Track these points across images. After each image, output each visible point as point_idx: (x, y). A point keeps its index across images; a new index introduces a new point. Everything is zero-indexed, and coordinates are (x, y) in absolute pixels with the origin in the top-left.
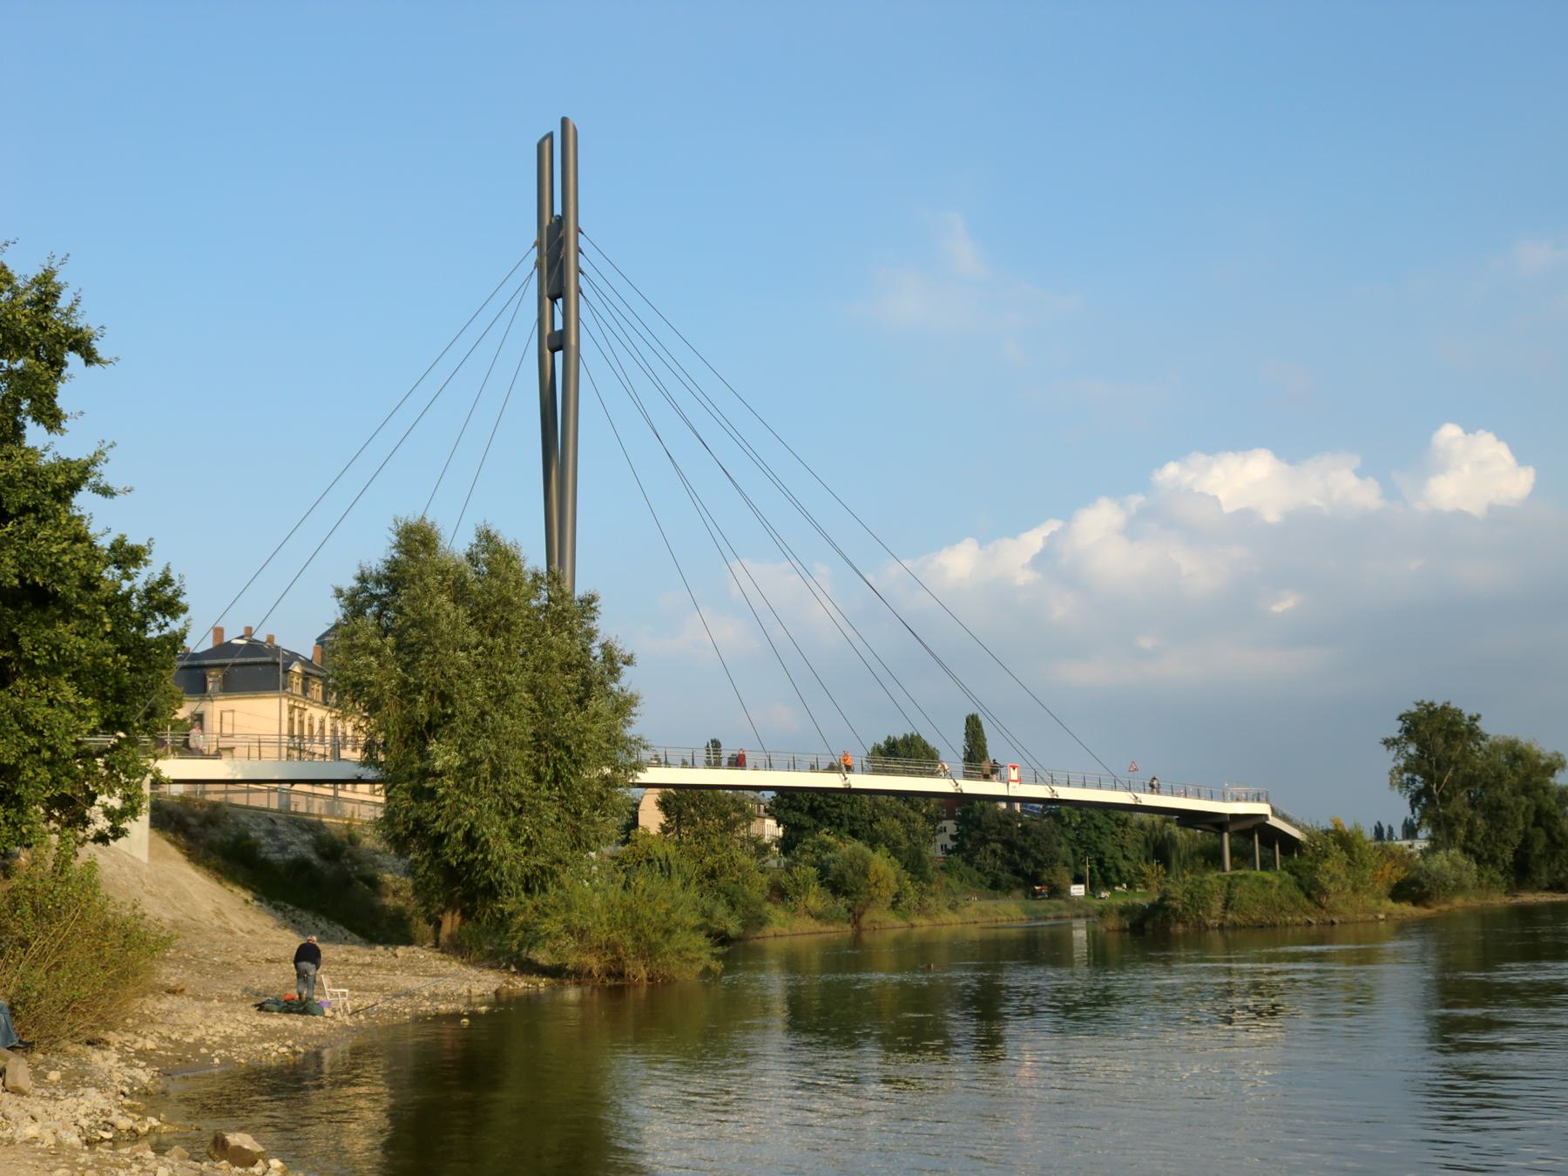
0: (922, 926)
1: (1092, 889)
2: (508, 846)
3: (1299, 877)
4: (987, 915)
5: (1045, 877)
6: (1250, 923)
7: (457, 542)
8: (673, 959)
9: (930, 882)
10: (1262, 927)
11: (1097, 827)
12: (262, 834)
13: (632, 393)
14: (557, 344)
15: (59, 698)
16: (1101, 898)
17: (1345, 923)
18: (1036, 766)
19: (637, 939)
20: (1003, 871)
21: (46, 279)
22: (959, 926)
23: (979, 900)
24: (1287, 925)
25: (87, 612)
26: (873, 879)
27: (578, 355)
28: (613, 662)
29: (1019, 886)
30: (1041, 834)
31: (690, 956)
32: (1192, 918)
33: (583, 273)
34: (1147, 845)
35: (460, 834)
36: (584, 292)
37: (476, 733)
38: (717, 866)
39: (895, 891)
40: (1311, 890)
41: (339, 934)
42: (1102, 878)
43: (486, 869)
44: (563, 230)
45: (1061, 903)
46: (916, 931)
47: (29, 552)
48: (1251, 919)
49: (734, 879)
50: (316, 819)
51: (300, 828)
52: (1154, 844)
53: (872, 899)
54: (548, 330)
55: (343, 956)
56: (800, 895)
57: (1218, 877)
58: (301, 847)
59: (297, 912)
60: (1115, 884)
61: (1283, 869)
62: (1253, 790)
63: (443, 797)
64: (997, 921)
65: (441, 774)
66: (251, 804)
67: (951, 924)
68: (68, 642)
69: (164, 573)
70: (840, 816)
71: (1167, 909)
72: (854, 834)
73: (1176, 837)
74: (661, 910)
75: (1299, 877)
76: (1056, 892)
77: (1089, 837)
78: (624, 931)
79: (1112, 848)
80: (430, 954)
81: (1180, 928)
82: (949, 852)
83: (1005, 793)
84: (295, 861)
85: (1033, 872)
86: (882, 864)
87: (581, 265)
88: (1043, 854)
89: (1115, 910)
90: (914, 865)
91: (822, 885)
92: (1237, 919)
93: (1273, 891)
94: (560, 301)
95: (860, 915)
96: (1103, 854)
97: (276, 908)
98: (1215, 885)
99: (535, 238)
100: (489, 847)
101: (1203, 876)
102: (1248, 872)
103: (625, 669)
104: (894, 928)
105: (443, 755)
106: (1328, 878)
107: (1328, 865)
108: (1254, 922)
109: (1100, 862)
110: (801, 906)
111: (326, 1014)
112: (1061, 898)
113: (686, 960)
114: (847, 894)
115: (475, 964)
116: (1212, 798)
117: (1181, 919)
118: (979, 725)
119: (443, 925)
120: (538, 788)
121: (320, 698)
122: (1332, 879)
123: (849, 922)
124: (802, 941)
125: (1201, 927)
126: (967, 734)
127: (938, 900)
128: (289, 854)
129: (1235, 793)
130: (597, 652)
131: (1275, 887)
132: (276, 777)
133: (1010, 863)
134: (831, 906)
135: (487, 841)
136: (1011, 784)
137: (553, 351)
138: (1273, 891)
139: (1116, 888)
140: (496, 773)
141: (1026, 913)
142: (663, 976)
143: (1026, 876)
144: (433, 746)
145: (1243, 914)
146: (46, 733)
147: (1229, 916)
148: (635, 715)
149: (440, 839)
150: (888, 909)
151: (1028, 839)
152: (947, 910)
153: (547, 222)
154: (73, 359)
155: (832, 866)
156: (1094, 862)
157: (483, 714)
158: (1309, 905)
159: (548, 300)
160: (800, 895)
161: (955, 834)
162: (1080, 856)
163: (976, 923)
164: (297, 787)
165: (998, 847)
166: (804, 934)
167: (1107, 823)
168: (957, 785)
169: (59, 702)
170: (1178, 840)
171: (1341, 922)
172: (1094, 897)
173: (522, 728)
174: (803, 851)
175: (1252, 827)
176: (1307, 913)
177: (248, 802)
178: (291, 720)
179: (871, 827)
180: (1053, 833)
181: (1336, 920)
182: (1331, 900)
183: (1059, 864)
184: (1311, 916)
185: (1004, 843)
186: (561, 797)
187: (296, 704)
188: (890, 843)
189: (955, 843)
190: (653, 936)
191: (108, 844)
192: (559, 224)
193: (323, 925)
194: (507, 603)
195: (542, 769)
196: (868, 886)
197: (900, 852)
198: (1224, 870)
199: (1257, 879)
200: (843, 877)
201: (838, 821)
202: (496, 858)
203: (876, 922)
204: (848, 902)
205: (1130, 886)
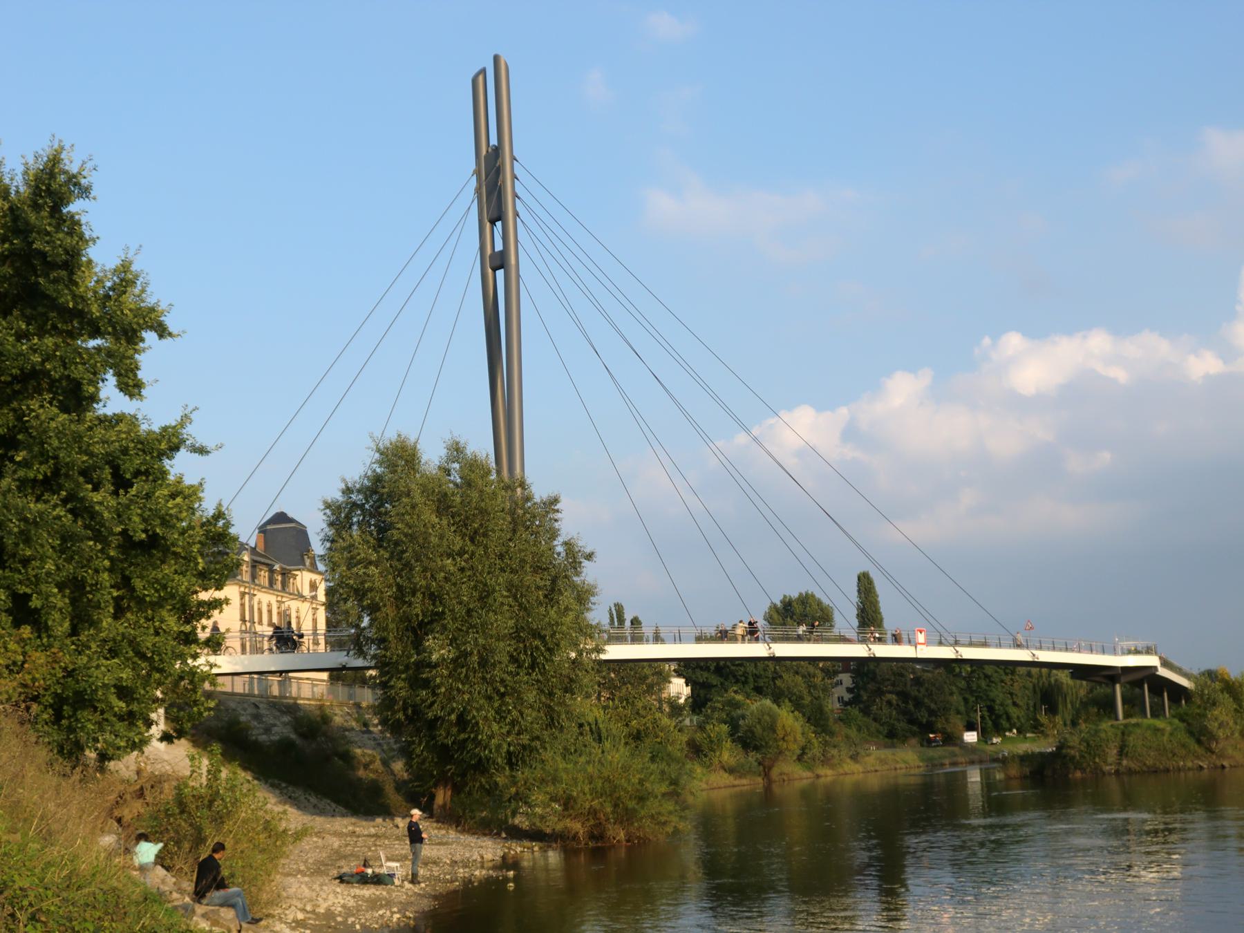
0: (826, 776)
1: (984, 736)
2: (495, 727)
3: (1189, 724)
4: (886, 763)
5: (939, 726)
6: (1145, 769)
7: (432, 455)
8: (647, 822)
9: (832, 734)
10: (1156, 772)
11: (987, 676)
12: (249, 718)
13: (570, 311)
14: (498, 263)
15: (164, 627)
16: (992, 744)
17: (1235, 767)
18: (940, 629)
19: (616, 806)
20: (898, 720)
21: (125, 267)
22: (861, 775)
23: (877, 749)
24: (1179, 770)
25: (182, 555)
26: (781, 733)
27: (518, 276)
28: (575, 557)
29: (914, 734)
30: (934, 685)
31: (663, 819)
32: (1089, 765)
33: (519, 198)
34: (1035, 692)
35: (453, 717)
36: (520, 215)
37: (464, 628)
38: (642, 728)
39: (801, 744)
40: (1201, 736)
41: (329, 807)
42: (993, 724)
43: (476, 747)
44: (500, 159)
45: (956, 749)
46: (822, 780)
47: (150, 510)
48: (1145, 764)
49: (659, 740)
50: (292, 701)
51: (280, 711)
52: (1041, 691)
53: (781, 753)
54: (489, 251)
55: (350, 828)
56: (714, 751)
57: (1112, 726)
58: (281, 729)
59: (290, 788)
60: (1005, 730)
61: (1174, 717)
62: (1141, 644)
63: (439, 687)
64: (896, 769)
65: (436, 665)
66: (236, 691)
67: (853, 773)
68: (173, 581)
69: (217, 508)
70: (745, 674)
71: (1065, 757)
72: (759, 690)
73: (1062, 683)
74: (635, 780)
75: (1189, 724)
76: (951, 739)
77: (979, 687)
78: (604, 798)
79: (1001, 695)
80: (428, 824)
81: (1078, 774)
82: (846, 704)
83: (914, 656)
84: (280, 741)
85: (927, 722)
86: (788, 719)
87: (517, 191)
88: (936, 704)
89: (1016, 759)
90: (816, 719)
91: (733, 741)
92: (1133, 765)
93: (1165, 738)
94: (499, 224)
95: (770, 768)
96: (994, 701)
97: (272, 785)
98: (1110, 734)
99: (473, 166)
100: (479, 728)
101: (1097, 725)
102: (1140, 720)
103: (585, 563)
104: (801, 779)
105: (438, 649)
106: (1216, 724)
107: (1216, 712)
108: (1148, 767)
109: (991, 709)
110: (716, 761)
111: (396, 884)
112: (955, 745)
113: (658, 823)
114: (757, 748)
115: (471, 831)
116: (1103, 652)
117: (1078, 766)
118: (870, 582)
119: (437, 797)
120: (518, 674)
121: (267, 584)
122: (1221, 725)
123: (760, 775)
124: (718, 795)
125: (1098, 774)
126: (859, 591)
127: (840, 751)
128: (274, 735)
129: (1125, 647)
130: (560, 549)
131: (1167, 734)
132: (273, 669)
133: (905, 712)
134: (742, 760)
135: (477, 723)
136: (919, 646)
137: (494, 270)
138: (1165, 738)
139: (1007, 734)
140: (483, 663)
141: (922, 760)
142: (639, 838)
143: (920, 725)
144: (429, 642)
145: (1137, 760)
146: (156, 658)
147: (1125, 762)
148: (594, 604)
149: (433, 724)
150: (794, 761)
151: (922, 690)
152: (848, 760)
153: (484, 152)
154: (150, 337)
155: (741, 722)
156: (985, 709)
157: (469, 612)
158: (1200, 751)
159: (488, 224)
160: (714, 751)
161: (851, 686)
162: (971, 704)
163: (876, 771)
164: (291, 674)
165: (893, 697)
166: (719, 788)
167: (996, 672)
168: (870, 649)
169: (164, 631)
170: (1065, 686)
171: (1231, 766)
172: (986, 742)
173: (503, 622)
174: (714, 709)
175: (1145, 676)
176: (1198, 757)
177: (233, 689)
178: (243, 605)
179: (775, 684)
180: (945, 683)
181: (1226, 763)
182: (1220, 746)
183: (952, 712)
184: (1202, 761)
185: (898, 694)
186: (538, 681)
187: (247, 590)
188: (794, 698)
189: (851, 696)
190: (630, 803)
191: (172, 742)
192: (496, 152)
193: (313, 800)
194: (483, 512)
195: (522, 657)
196: (776, 740)
197: (803, 706)
198: (1117, 719)
199: (1149, 727)
200: (752, 732)
201: (743, 679)
202: (485, 737)
203: (784, 774)
204: (759, 756)
205: (1019, 732)
